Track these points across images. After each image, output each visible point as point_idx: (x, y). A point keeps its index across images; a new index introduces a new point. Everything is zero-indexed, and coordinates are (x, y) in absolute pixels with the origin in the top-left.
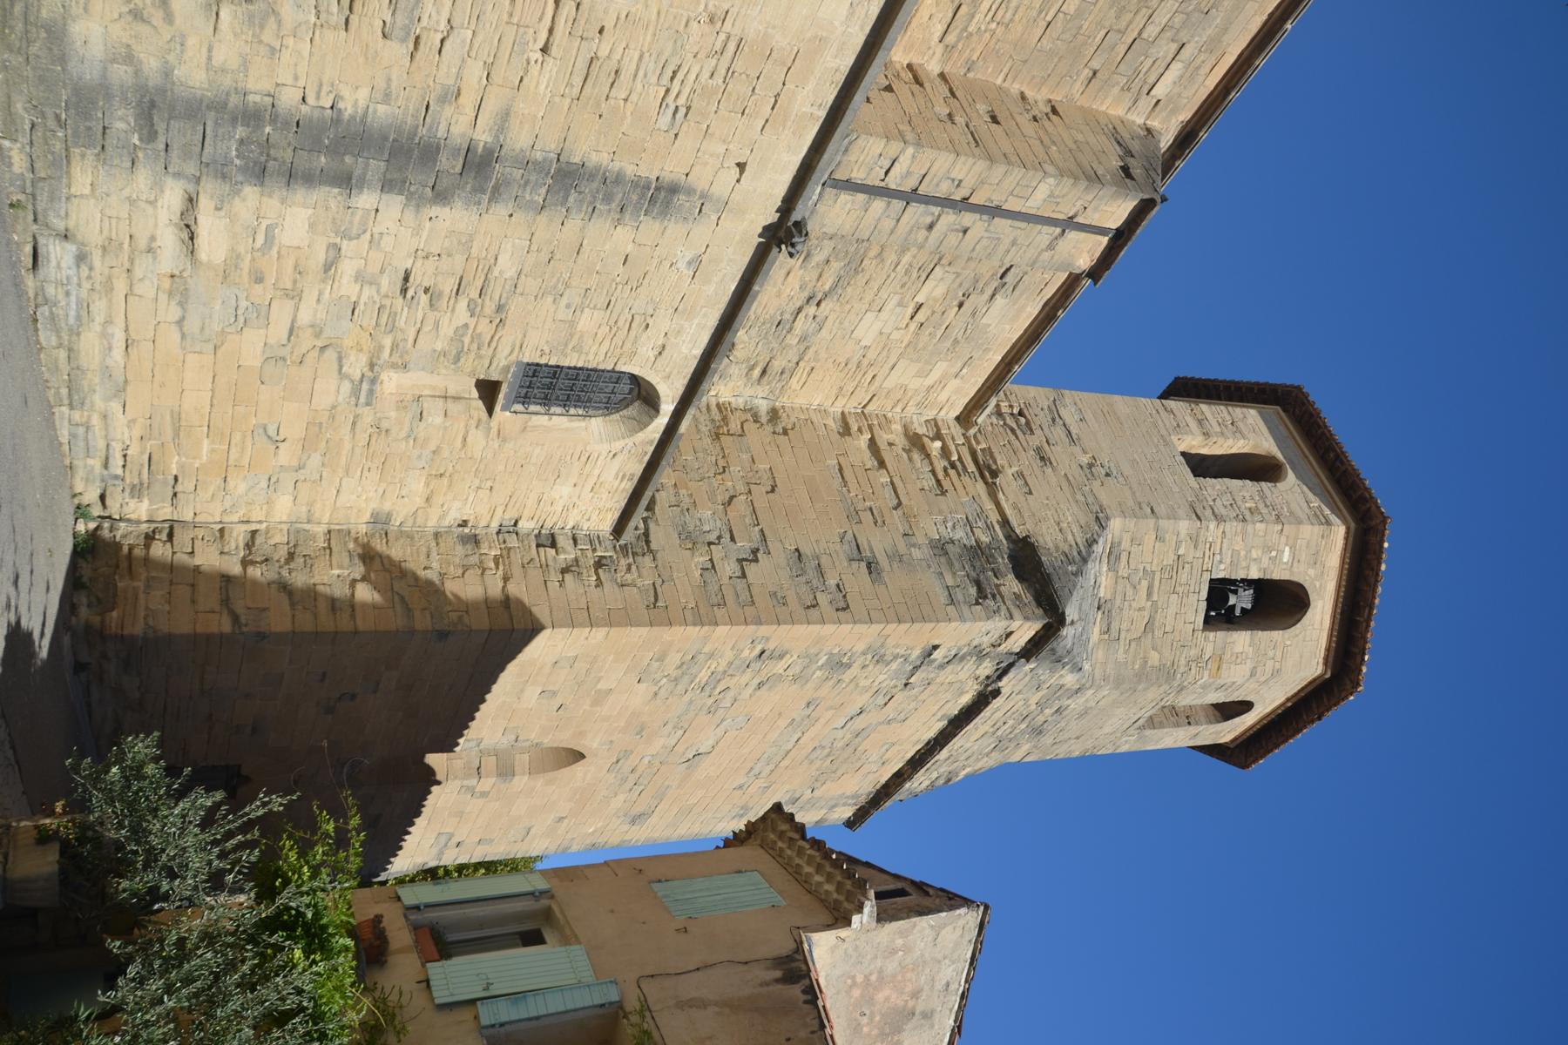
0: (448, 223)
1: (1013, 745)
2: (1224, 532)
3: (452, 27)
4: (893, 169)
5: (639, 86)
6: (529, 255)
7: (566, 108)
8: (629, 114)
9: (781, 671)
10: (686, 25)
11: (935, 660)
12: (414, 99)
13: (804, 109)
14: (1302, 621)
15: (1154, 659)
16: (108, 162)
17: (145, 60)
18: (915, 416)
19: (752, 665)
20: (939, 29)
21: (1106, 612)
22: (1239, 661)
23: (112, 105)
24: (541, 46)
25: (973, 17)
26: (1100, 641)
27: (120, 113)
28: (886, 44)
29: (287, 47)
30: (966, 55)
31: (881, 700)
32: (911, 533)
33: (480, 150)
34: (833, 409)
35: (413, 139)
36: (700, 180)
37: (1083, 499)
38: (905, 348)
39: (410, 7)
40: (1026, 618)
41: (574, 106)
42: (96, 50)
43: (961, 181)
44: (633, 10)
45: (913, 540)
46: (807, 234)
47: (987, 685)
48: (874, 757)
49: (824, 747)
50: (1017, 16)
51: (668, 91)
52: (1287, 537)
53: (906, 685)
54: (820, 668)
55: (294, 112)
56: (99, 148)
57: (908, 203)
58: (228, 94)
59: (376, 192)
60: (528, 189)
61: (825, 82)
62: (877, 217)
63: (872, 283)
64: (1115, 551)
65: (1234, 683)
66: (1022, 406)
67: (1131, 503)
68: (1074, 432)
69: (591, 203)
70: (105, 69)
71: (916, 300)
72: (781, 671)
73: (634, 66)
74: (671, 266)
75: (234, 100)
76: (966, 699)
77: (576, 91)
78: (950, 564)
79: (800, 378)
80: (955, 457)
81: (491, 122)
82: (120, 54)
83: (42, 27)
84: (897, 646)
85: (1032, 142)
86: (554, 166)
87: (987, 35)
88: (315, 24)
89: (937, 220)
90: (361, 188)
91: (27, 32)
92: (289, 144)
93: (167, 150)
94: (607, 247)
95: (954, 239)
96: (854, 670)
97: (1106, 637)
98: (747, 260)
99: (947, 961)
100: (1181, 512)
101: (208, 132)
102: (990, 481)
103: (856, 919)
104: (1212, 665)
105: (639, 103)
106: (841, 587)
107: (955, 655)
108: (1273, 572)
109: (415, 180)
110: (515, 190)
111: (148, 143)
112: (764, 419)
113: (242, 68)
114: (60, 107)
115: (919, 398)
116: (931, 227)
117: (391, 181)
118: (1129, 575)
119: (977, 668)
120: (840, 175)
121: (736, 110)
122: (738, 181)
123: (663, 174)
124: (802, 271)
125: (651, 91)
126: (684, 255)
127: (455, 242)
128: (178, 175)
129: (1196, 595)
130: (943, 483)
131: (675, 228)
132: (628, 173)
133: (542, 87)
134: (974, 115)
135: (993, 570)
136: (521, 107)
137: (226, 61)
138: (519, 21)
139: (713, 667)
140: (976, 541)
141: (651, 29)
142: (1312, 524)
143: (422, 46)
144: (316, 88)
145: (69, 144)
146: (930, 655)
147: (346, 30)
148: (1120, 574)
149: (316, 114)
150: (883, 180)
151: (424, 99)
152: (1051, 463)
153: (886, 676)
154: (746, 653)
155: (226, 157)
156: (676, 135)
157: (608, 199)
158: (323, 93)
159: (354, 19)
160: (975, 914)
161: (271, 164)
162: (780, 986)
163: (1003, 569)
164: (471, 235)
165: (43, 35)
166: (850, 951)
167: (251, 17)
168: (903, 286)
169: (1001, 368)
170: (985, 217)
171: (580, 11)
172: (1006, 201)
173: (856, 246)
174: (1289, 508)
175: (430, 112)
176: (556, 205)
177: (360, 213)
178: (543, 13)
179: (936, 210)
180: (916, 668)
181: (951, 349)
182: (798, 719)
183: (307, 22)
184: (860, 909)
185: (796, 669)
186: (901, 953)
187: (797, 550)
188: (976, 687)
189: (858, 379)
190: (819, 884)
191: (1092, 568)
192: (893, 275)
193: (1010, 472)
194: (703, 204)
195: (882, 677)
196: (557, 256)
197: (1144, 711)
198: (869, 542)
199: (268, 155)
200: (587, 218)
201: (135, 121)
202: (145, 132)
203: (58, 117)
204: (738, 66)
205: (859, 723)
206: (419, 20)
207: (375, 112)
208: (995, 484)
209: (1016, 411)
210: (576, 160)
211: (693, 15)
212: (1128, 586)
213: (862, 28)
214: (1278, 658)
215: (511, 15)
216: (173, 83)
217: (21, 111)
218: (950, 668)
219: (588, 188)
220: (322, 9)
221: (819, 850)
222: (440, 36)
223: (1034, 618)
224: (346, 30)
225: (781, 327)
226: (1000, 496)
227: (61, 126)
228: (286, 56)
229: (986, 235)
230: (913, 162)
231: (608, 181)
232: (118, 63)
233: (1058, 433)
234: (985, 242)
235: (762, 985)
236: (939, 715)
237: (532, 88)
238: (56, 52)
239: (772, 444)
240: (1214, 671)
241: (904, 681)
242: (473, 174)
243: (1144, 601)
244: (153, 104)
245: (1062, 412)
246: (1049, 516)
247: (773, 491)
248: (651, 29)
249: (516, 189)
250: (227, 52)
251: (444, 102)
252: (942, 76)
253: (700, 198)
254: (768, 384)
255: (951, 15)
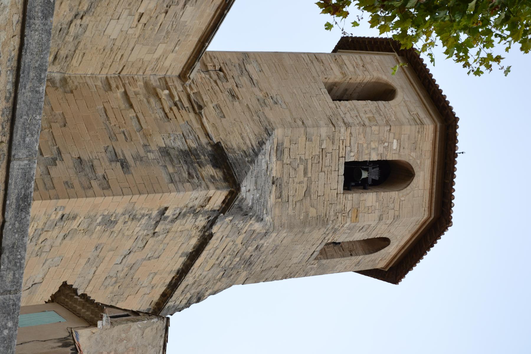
1: (235, 273)
2: (351, 133)
9: (76, 227)
11: (168, 217)
14: (410, 185)
15: (313, 212)
18: (152, 77)
19: (58, 224)
21: (278, 185)
22: (370, 212)
26: (276, 203)
31: (140, 244)
32: (147, 144)
34: (100, 76)
37: (258, 118)
38: (138, 38)
40: (217, 189)
45: (149, 148)
47: (205, 232)
48: (145, 283)
49: (111, 277)
52: (394, 134)
53: (154, 233)
54: (99, 224)
64: (280, 148)
65: (369, 226)
66: (222, 65)
67: (289, 119)
68: (255, 77)
71: (139, 11)
72: (76, 227)
76: (194, 241)
78: (172, 161)
79: (78, 60)
80: (177, 99)
84: (142, 209)
96: (119, 225)
97: (280, 200)
99: (150, 346)
100: (322, 123)
102: (198, 112)
103: (99, 323)
104: (352, 215)
106: (106, 176)
107: (180, 213)
108: (387, 155)
112: (58, 85)
115: (152, 66)
118: (291, 162)
119: (195, 221)
129: (337, 172)
130: (169, 115)
135: (198, 163)
139: (35, 226)
140: (188, 147)
142: (410, 125)
146: (164, 214)
148: (285, 162)
152: (238, 98)
153: (140, 228)
154: (53, 217)
160: (162, 322)
162: (60, 348)
163: (204, 162)
166: (98, 339)
169: (199, 45)
174: (395, 115)
180: (157, 223)
181: (166, 36)
182: (92, 258)
184: (101, 318)
185: (85, 226)
186: (125, 341)
187: (79, 158)
188: (198, 234)
189: (113, 57)
190: (80, 310)
191: (262, 160)
193: (211, 106)
195: (137, 229)
197: (315, 246)
198: (122, 151)
205: (130, 259)
208: (201, 113)
209: (217, 68)
212: (291, 169)
214: (397, 208)
218: (178, 222)
221: (84, 299)
223: (223, 188)
225: (62, 32)
226: (204, 120)
233: (245, 80)
235: (52, 348)
236: (180, 252)
239: (64, 99)
240: (354, 218)
241: (152, 231)
243: (303, 177)
245: (248, 67)
246: (235, 129)
247: (65, 126)
254: (59, 64)
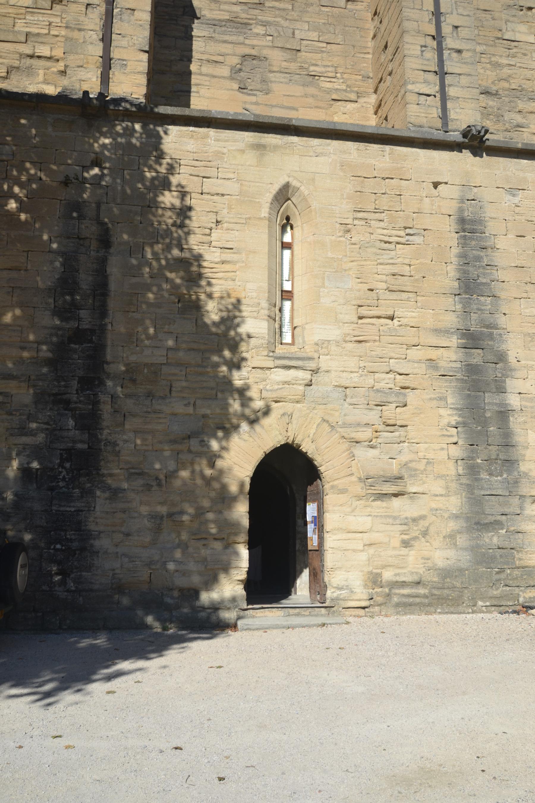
0: (519, 351)
3: (390, 371)
4: (425, 93)
5: (399, 260)
6: (531, 297)
7: (424, 298)
8: (418, 261)
10: (355, 244)
12: (440, 384)
13: (388, 160)
16: (521, 546)
17: (451, 528)
20: (350, 106)
23: (483, 544)
24: (390, 321)
25: (337, 89)
27: (487, 540)
28: (331, 127)
29: (425, 456)
30: (361, 83)
33: (464, 341)
35: (466, 380)
36: (451, 207)
39: (384, 395)
41: (422, 294)
42: (451, 553)
43: (422, 46)
44: (354, 276)
46: (469, 126)
50: (329, 64)
51: (398, 243)
55: (464, 448)
56: (513, 551)
57: (446, 74)
58: (461, 484)
59: (506, 396)
60: (483, 308)
61: (367, 154)
62: (461, 89)
63: (529, 76)
69: (484, 268)
70: (461, 549)
73: (388, 267)
74: (518, 206)
75: (464, 481)
77: (411, 295)
81: (442, 338)
82: (450, 541)
83: (444, 580)
85: (390, 15)
86: (463, 296)
87: (345, 76)
88: (408, 443)
89: (453, 49)
90: (506, 405)
91: (448, 588)
92: (486, 448)
93: (506, 515)
94: (514, 250)
95: (463, 33)
98: (501, 160)
101: (488, 493)
105: (409, 257)
109: (493, 375)
110: (486, 316)
111: (504, 525)
113: (443, 478)
114: (491, 571)
116: (459, 51)
117: (497, 388)
120: (439, 124)
121: (399, 199)
122: (446, 183)
123: (453, 230)
124: (531, 126)
125: (400, 253)
126: (508, 200)
127: (532, 344)
128: (522, 508)
131: (489, 212)
132: (457, 251)
133: (414, 314)
134: (387, 60)
136: (429, 323)
137: (441, 487)
138: (377, 335)
141: (362, 263)
143: (406, 385)
144: (446, 438)
145: (514, 566)
147: (406, 426)
149: (463, 436)
150: (435, 96)
151: (438, 378)
155: (503, 482)
156: (425, 230)
157: (478, 259)
158: (449, 434)
159: (399, 423)
161: (502, 456)
164: (525, 335)
165: (448, 580)
167: (411, 476)
168: (525, 55)
170: (442, 19)
171: (362, 304)
172: (427, 10)
173: (503, 98)
175: (445, 374)
176: (490, 289)
177: (524, 403)
178: (369, 324)
179: (446, 53)
183: (408, 447)
192: (518, 65)
194: (468, 200)
196: (528, 280)
199: (496, 459)
200: (496, 268)
201: (491, 532)
202: (497, 527)
203: (498, 573)
204: (371, 208)
206: (391, 389)
207: (453, 404)
210: (456, 284)
211: (348, 242)
213: (329, 145)
215: (375, 341)
216: (462, 513)
217: (499, 591)
219: (473, 272)
220: (399, 441)
222: (398, 377)
224: (406, 426)
227: (504, 571)
228: (430, 456)
229: (455, 12)
230: (417, 82)
231: (466, 262)
232: (456, 542)
234: (460, 11)
237: (416, 320)
238: (457, 574)
242: (481, 342)
244: (477, 523)
248: (362, 263)
249: (485, 315)
250: (437, 487)
251: (437, 367)
252: (375, 92)
253: (464, 203)
255: (340, 103)
